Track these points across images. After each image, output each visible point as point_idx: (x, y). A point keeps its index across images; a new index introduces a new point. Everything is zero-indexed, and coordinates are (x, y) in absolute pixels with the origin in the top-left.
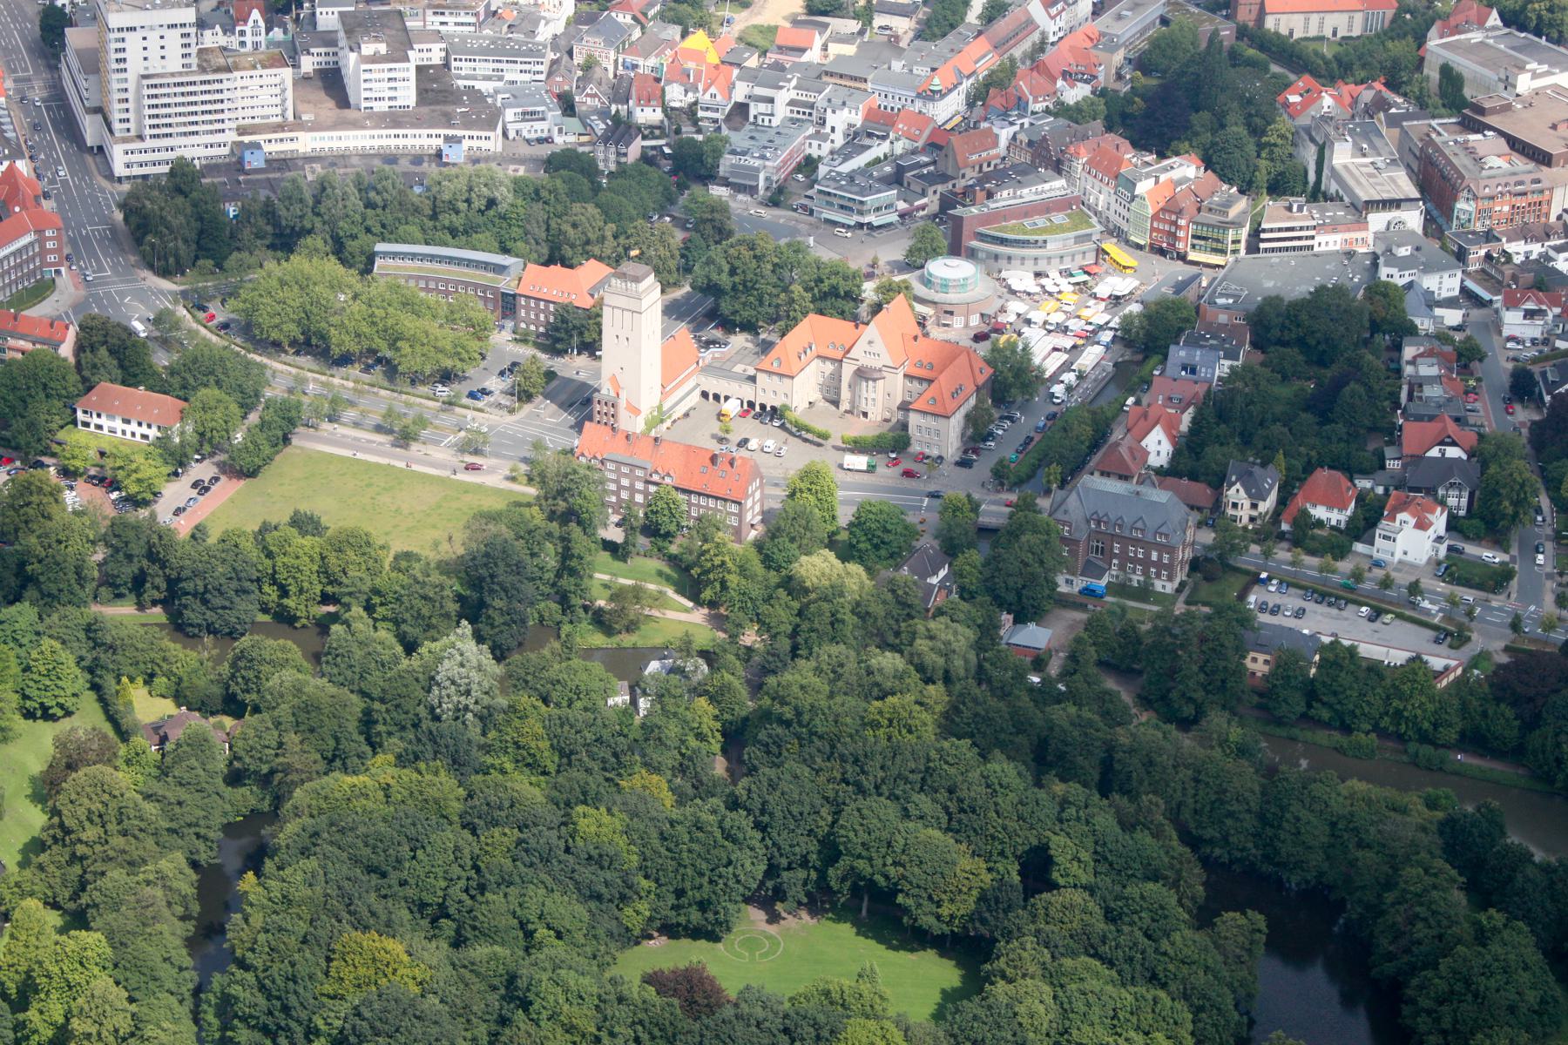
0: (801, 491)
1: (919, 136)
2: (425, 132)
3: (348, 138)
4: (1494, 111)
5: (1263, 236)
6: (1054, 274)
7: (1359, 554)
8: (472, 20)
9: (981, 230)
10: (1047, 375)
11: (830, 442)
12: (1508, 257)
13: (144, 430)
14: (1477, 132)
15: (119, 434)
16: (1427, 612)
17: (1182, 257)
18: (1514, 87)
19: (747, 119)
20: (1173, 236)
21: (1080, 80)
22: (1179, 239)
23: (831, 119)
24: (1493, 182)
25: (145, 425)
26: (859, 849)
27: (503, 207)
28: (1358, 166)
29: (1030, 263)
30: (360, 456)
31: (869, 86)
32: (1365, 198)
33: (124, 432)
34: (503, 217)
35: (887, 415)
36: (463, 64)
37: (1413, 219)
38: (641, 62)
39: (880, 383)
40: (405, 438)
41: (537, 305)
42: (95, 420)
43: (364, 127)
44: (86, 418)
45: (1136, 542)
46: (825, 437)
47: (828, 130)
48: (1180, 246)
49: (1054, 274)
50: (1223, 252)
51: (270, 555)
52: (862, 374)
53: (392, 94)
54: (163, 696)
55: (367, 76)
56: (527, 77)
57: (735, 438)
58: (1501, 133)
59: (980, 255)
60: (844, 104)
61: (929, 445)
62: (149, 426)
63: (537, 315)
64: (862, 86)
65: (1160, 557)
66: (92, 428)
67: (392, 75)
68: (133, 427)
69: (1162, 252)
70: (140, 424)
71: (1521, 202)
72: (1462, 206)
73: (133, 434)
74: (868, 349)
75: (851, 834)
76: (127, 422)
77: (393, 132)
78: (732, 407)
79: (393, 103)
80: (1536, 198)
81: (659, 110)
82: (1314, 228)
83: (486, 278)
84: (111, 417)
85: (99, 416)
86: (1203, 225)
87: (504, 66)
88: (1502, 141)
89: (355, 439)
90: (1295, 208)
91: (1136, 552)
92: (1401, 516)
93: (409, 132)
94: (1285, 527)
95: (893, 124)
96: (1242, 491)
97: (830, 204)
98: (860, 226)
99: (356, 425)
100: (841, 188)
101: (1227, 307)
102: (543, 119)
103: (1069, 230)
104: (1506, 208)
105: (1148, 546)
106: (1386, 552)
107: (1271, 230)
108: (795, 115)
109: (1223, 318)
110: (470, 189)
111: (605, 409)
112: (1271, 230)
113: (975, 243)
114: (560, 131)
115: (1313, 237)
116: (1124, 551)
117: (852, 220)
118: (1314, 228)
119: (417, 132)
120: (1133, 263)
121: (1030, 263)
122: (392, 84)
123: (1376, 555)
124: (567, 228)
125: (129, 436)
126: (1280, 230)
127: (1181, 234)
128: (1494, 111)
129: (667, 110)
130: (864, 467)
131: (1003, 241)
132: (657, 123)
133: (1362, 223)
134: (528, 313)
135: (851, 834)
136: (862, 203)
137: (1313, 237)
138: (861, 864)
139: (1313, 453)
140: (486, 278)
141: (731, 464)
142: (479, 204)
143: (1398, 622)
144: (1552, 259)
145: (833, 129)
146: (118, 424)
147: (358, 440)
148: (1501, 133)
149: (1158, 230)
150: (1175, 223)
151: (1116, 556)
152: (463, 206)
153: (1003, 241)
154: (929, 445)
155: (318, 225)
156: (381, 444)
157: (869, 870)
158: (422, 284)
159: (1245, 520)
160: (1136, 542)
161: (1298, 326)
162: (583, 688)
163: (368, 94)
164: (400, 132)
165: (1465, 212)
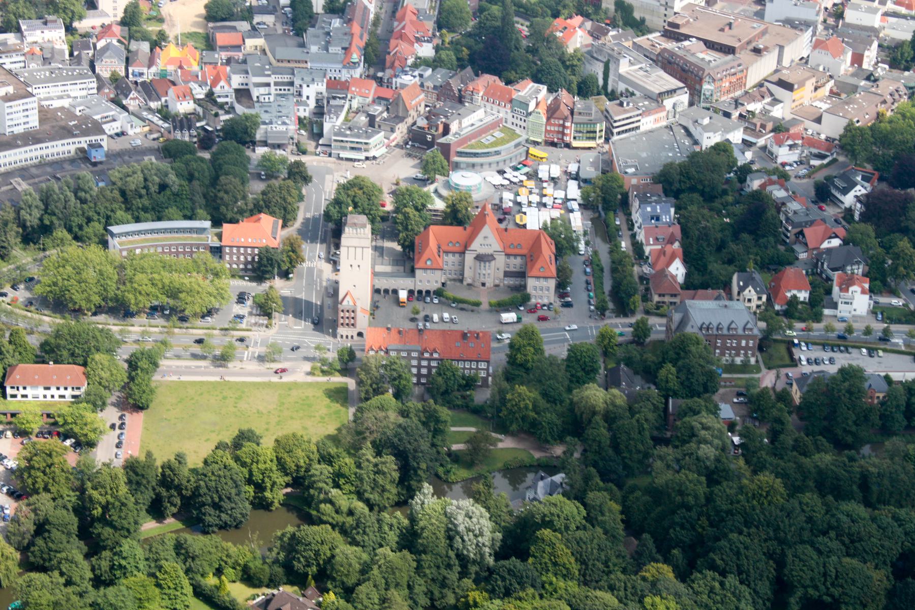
0: (524, 346)
1: (369, 94)
2: (59, 143)
3: (10, 155)
4: (684, 25)
5: (615, 125)
6: (508, 170)
7: (827, 316)
8: (22, 58)
9: (459, 149)
10: (110, 228)
11: (482, 307)
12: (752, 113)
13: (62, 392)
14: (685, 40)
15: (41, 398)
16: (897, 344)
17: (568, 146)
18: (673, 8)
19: (252, 99)
20: (563, 134)
21: (425, 41)
22: (567, 135)
23: (306, 91)
24: (720, 70)
25: (62, 389)
26: (808, 582)
27: (175, 188)
28: (635, 71)
29: (494, 166)
30: (184, 378)
31: (309, 65)
32: (658, 92)
33: (45, 396)
34: (176, 195)
35: (497, 282)
36: (41, 91)
37: (684, 98)
38: (145, 70)
39: (493, 263)
40: (222, 359)
41: (238, 251)
42: (22, 391)
43: (18, 146)
44: (14, 392)
45: (731, 337)
46: (477, 304)
47: (304, 98)
48: (567, 139)
49: (508, 170)
50: (594, 138)
51: (244, 464)
52: (480, 258)
53: (26, 120)
54: (234, 582)
55: (9, 110)
56: (84, 93)
57: (421, 315)
58: (698, 39)
59: (462, 166)
60: (313, 80)
61: (541, 297)
62: (66, 389)
63: (238, 258)
64: (304, 65)
65: (747, 343)
66: (19, 398)
67: (25, 107)
68: (53, 391)
69: (553, 144)
70: (58, 389)
71: (734, 79)
72: (707, 87)
73: (53, 396)
74: (483, 242)
75: (801, 573)
76: (48, 388)
77: (38, 146)
78: (403, 295)
79: (27, 126)
80: (739, 75)
81: (192, 102)
82: (641, 115)
83: (193, 238)
84: (34, 385)
85: (25, 388)
86: (580, 124)
87: (69, 87)
88: (701, 43)
89: (186, 367)
90: (625, 104)
91: (731, 344)
92: (851, 289)
93: (49, 144)
94: (777, 307)
95: (348, 89)
96: (753, 291)
97: (344, 148)
98: (367, 158)
99: (178, 357)
100: (346, 136)
101: (634, 174)
102: (114, 120)
103: (508, 142)
104: (727, 84)
105: (739, 338)
106: (846, 311)
107: (620, 120)
108: (278, 92)
109: (634, 181)
110: (146, 180)
111: (347, 314)
112: (620, 120)
113: (456, 159)
114: (132, 126)
115: (639, 121)
116: (724, 343)
117: (362, 156)
118: (641, 115)
119: (54, 143)
120: (544, 155)
121: (494, 166)
122: (26, 113)
123: (839, 315)
124: (221, 194)
125: (49, 398)
126: (623, 119)
127: (567, 131)
128: (684, 25)
129: (197, 102)
130: (515, 320)
131: (475, 155)
132: (192, 111)
133: (661, 107)
134: (231, 257)
135: (801, 573)
136: (366, 144)
137: (639, 121)
138: (811, 591)
139: (758, 258)
140: (193, 238)
141: (477, 337)
142: (154, 188)
143: (886, 354)
144: (769, 111)
145: (308, 98)
146: (40, 391)
147: (189, 367)
148: (698, 39)
149: (551, 131)
150: (564, 126)
151: (718, 348)
152: (143, 192)
153: (475, 155)
154: (541, 297)
155: (56, 222)
156: (205, 367)
157: (817, 594)
158: (160, 250)
159: (754, 308)
160: (731, 337)
161: (689, 179)
162: (569, 514)
163: (10, 123)
164: (43, 145)
165: (708, 90)
